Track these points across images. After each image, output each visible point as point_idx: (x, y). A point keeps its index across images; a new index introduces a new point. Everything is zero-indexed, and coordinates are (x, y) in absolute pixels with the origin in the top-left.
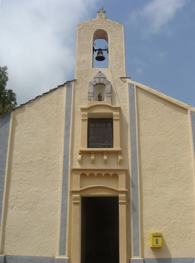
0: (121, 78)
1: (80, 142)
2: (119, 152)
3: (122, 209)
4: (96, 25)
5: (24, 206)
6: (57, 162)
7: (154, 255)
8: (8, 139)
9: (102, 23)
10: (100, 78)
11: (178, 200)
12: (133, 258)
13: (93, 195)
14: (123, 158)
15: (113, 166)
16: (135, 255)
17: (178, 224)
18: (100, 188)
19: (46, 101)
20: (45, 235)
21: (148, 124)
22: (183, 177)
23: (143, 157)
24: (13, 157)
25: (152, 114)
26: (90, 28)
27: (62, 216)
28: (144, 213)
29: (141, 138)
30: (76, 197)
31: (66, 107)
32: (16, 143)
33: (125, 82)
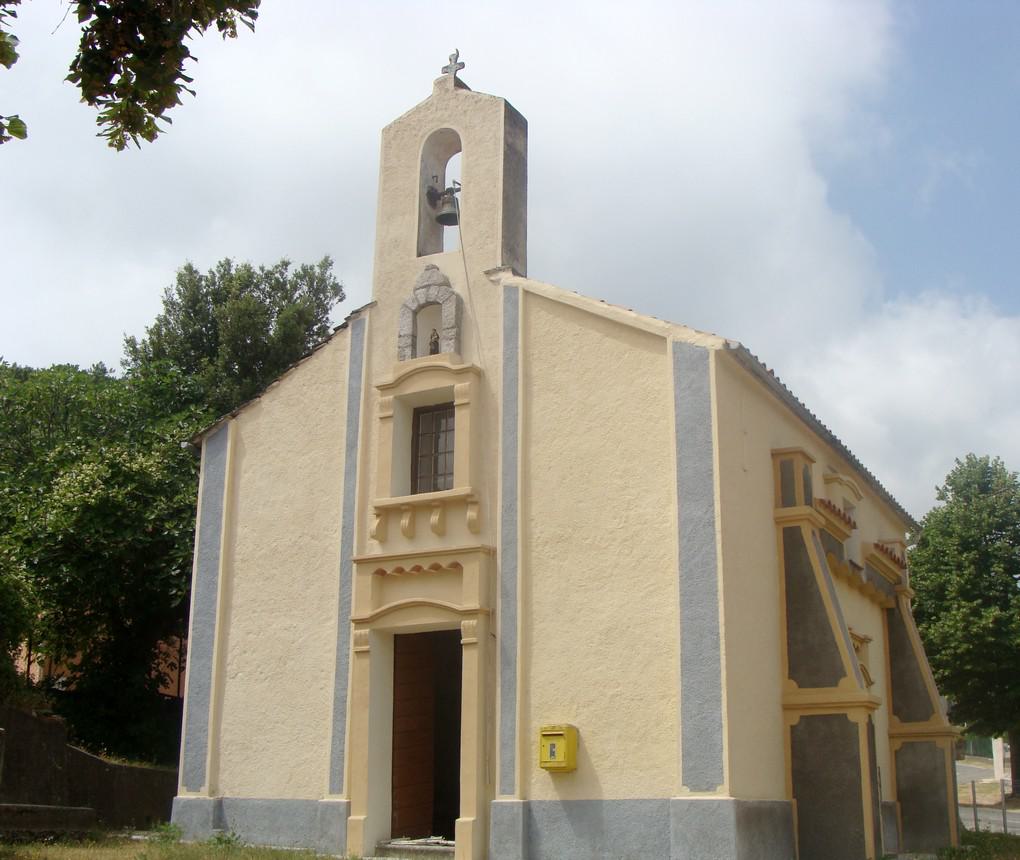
0: (487, 273)
1: (385, 481)
2: (469, 500)
3: (470, 662)
4: (431, 117)
5: (259, 670)
6: (331, 544)
7: (555, 793)
8: (222, 499)
9: (446, 109)
10: (428, 286)
11: (629, 627)
12: (501, 799)
13: (399, 628)
14: (478, 516)
15: (461, 540)
16: (503, 792)
17: (625, 699)
18: (427, 606)
19: (309, 377)
20: (302, 744)
21: (556, 403)
22: (645, 557)
23: (535, 510)
24: (235, 542)
25: (568, 370)
26: (414, 132)
27: (336, 690)
28: (534, 672)
29: (534, 449)
30: (361, 635)
31: (351, 388)
32: (243, 504)
33: (496, 282)
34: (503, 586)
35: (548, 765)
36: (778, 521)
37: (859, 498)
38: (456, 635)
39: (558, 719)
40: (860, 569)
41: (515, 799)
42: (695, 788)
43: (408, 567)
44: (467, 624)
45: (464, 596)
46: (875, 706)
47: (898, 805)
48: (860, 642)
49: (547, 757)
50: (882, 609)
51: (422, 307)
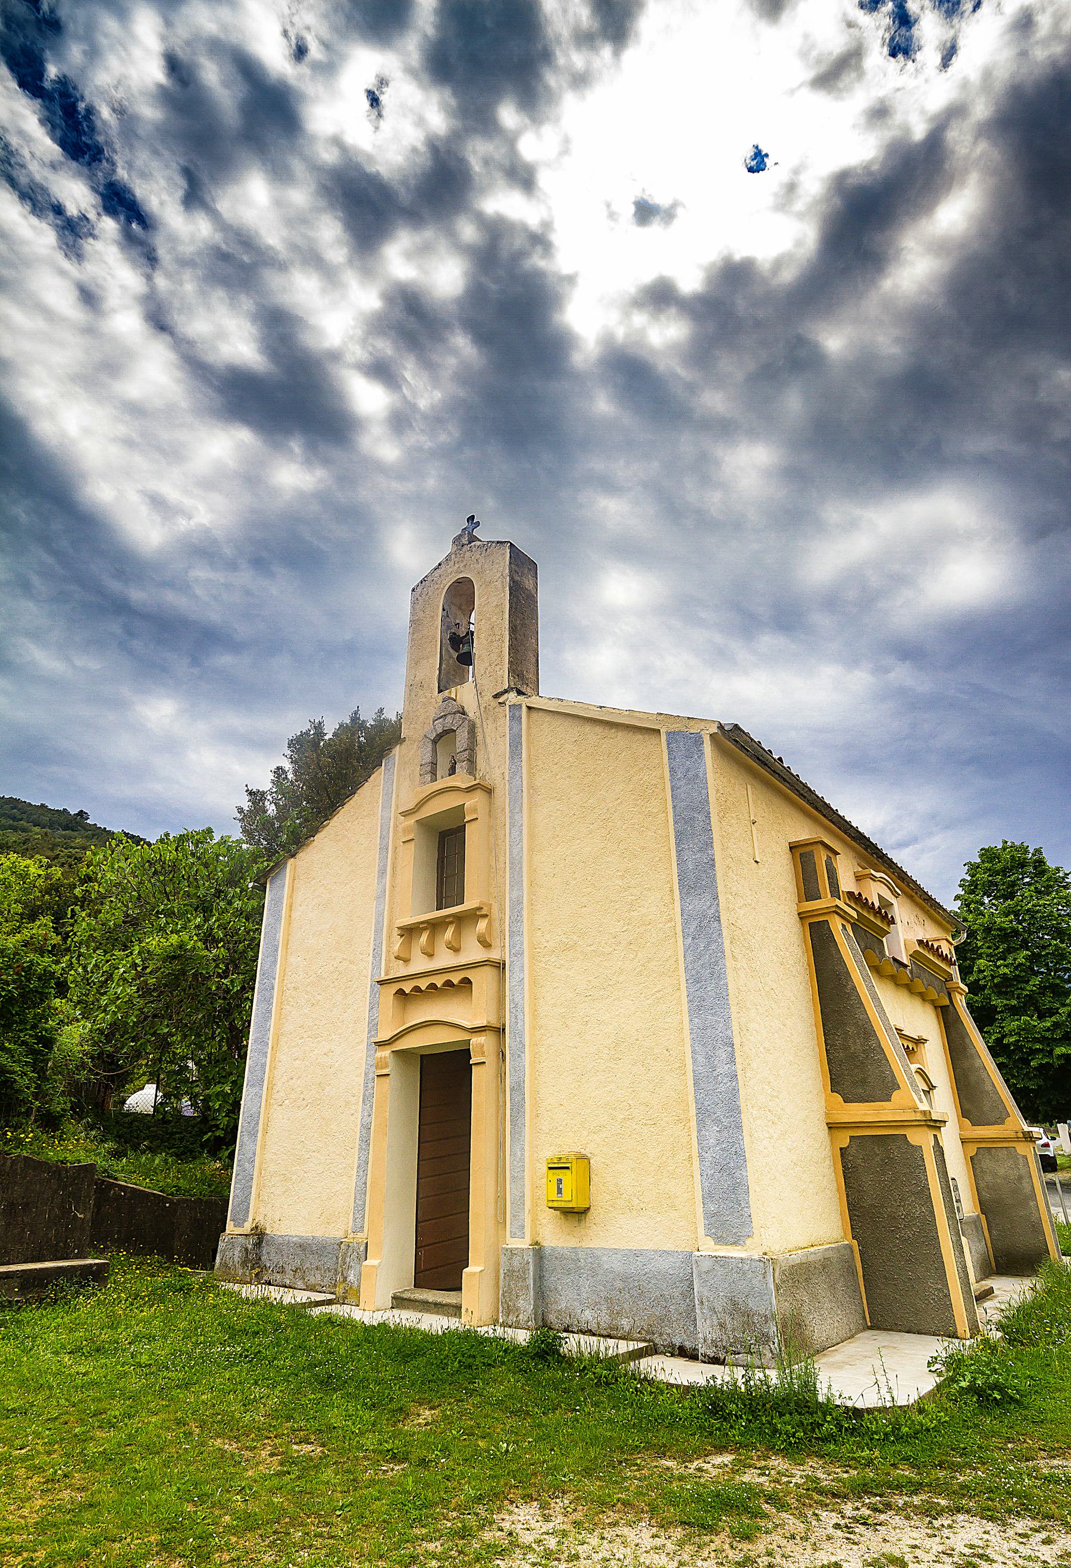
15: (473, 952)
34: (512, 1001)
35: (555, 1205)
36: (802, 916)
37: (896, 896)
38: (466, 1054)
39: (567, 1145)
40: (906, 966)
41: (522, 1244)
42: (719, 1240)
43: (439, 981)
44: (476, 1040)
45: (465, 1014)
46: (942, 1124)
47: (983, 1217)
48: (913, 1046)
49: (554, 1195)
50: (936, 1007)
51: (440, 736)
